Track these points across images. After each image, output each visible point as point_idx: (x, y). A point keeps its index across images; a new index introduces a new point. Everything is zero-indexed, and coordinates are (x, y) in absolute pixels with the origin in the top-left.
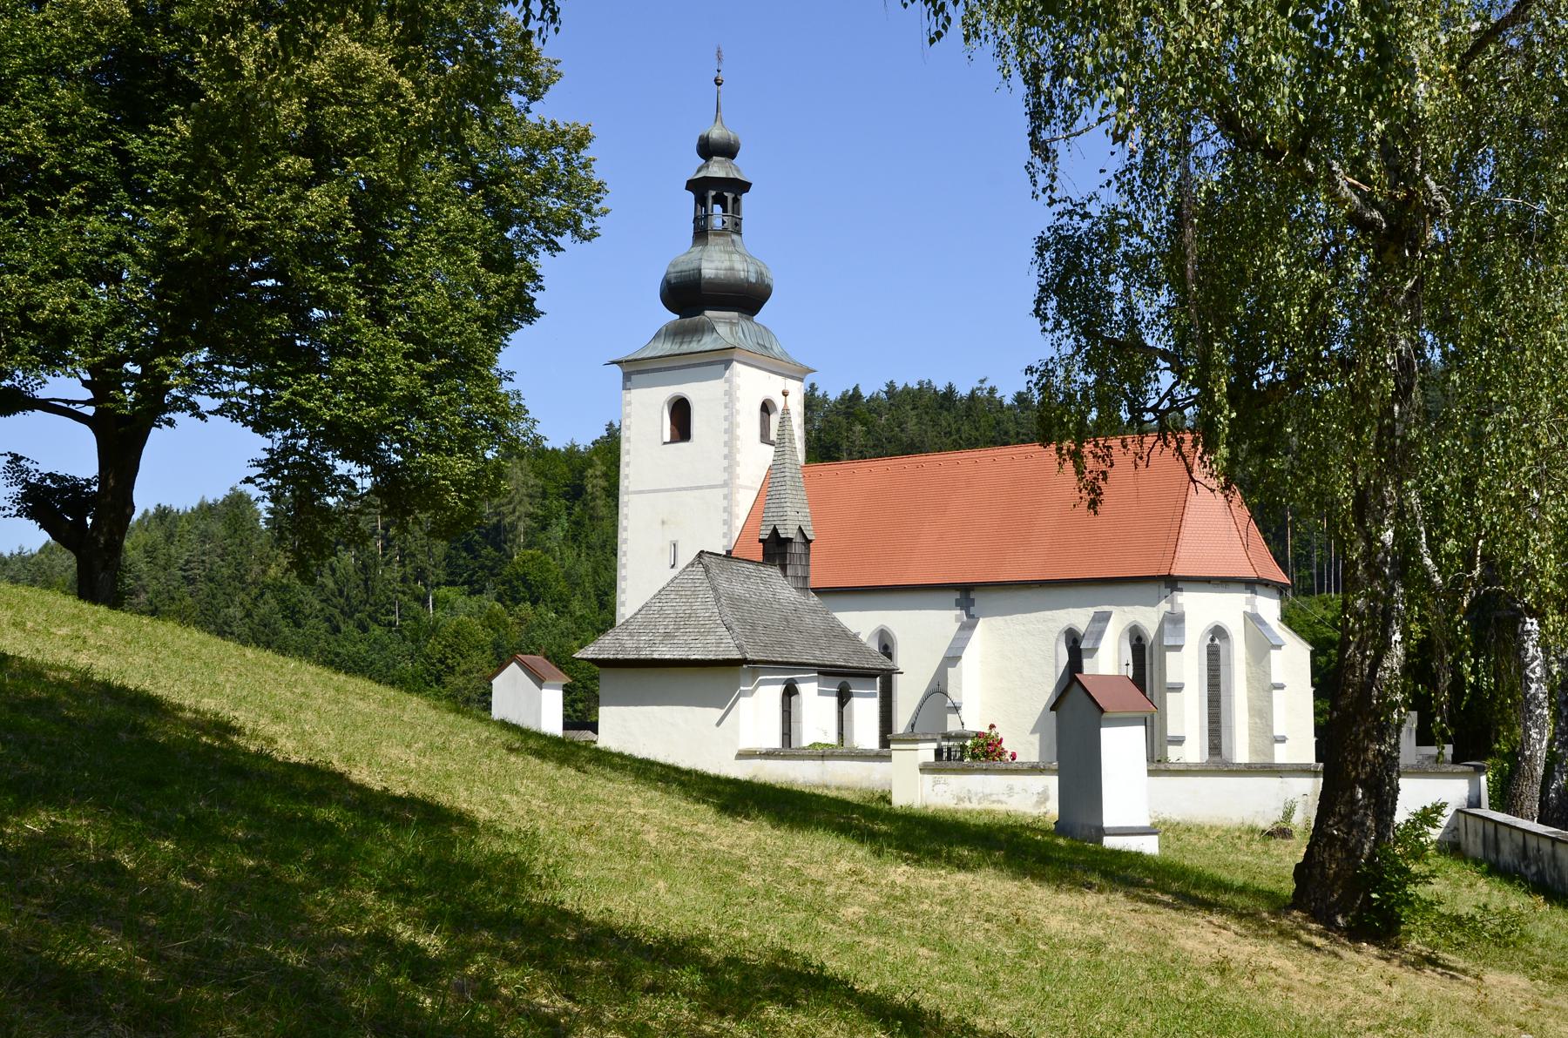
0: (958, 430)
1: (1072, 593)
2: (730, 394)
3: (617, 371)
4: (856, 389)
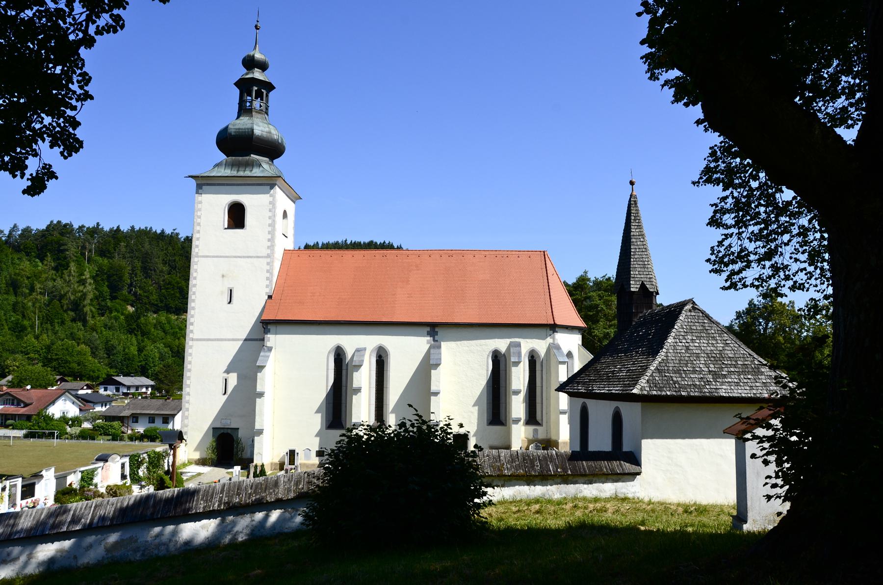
0: (166, 249)
1: (497, 331)
2: (273, 203)
3: (193, 183)
4: (118, 227)
